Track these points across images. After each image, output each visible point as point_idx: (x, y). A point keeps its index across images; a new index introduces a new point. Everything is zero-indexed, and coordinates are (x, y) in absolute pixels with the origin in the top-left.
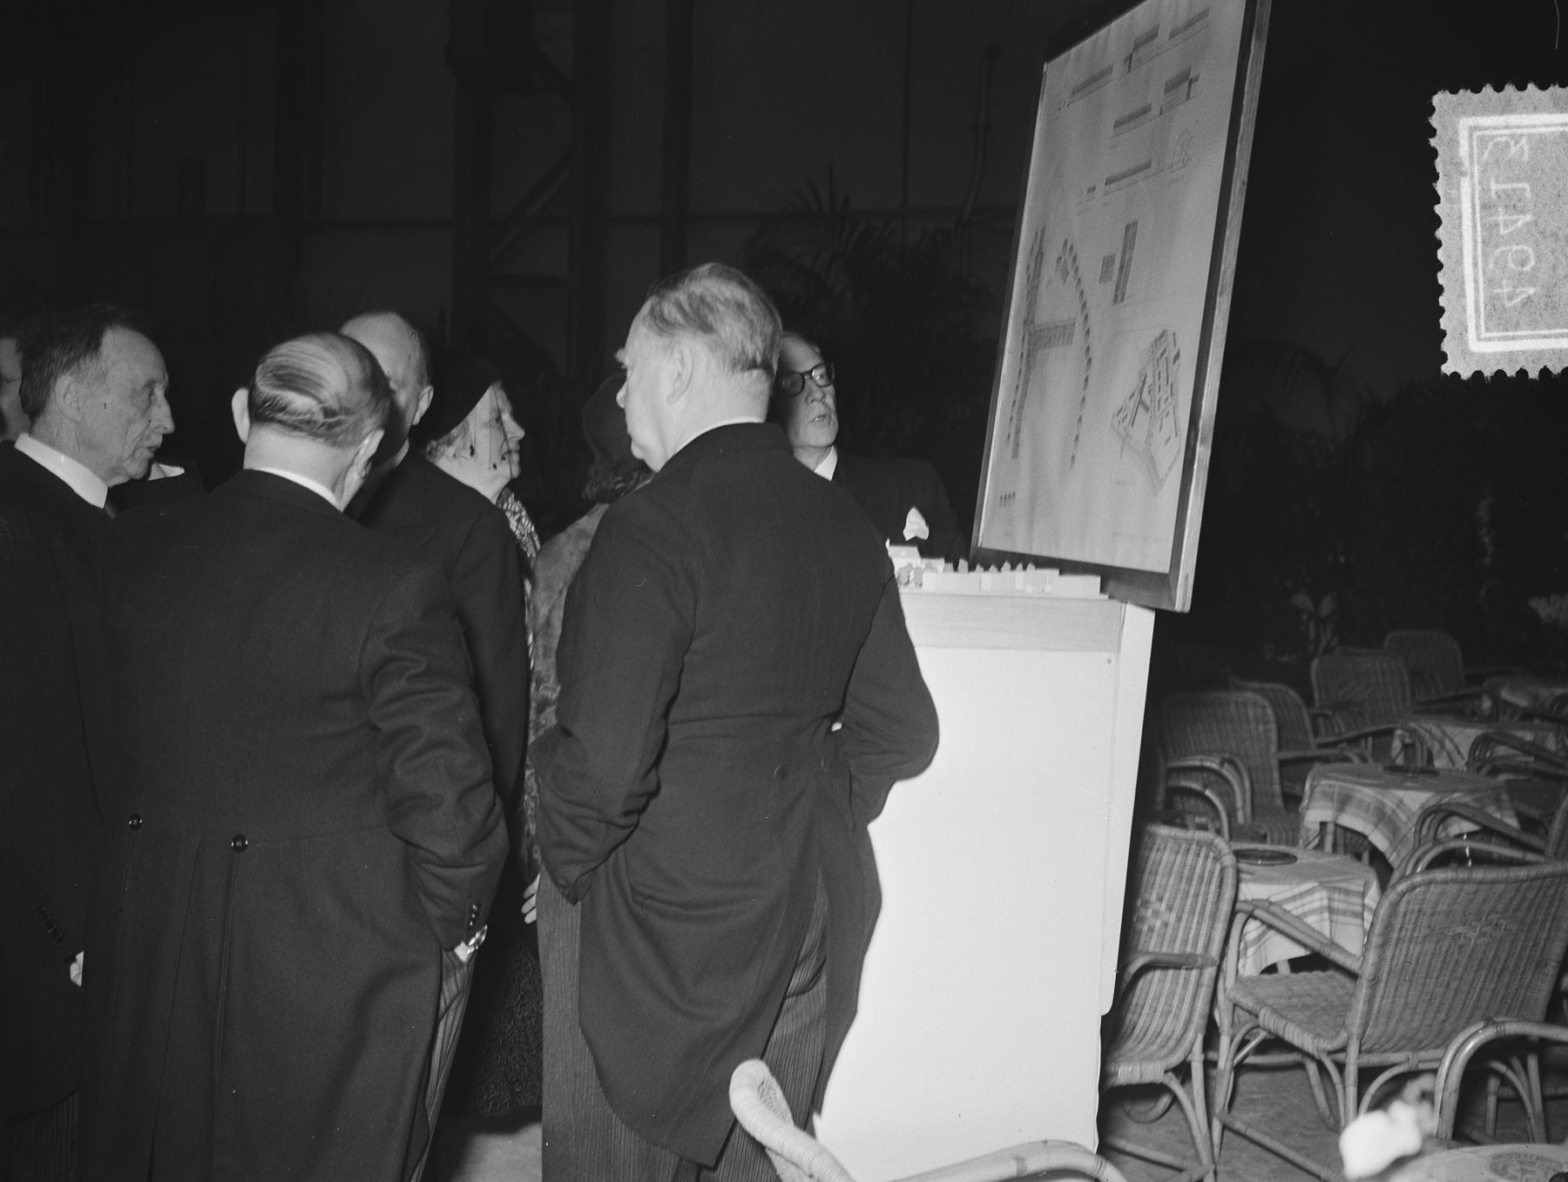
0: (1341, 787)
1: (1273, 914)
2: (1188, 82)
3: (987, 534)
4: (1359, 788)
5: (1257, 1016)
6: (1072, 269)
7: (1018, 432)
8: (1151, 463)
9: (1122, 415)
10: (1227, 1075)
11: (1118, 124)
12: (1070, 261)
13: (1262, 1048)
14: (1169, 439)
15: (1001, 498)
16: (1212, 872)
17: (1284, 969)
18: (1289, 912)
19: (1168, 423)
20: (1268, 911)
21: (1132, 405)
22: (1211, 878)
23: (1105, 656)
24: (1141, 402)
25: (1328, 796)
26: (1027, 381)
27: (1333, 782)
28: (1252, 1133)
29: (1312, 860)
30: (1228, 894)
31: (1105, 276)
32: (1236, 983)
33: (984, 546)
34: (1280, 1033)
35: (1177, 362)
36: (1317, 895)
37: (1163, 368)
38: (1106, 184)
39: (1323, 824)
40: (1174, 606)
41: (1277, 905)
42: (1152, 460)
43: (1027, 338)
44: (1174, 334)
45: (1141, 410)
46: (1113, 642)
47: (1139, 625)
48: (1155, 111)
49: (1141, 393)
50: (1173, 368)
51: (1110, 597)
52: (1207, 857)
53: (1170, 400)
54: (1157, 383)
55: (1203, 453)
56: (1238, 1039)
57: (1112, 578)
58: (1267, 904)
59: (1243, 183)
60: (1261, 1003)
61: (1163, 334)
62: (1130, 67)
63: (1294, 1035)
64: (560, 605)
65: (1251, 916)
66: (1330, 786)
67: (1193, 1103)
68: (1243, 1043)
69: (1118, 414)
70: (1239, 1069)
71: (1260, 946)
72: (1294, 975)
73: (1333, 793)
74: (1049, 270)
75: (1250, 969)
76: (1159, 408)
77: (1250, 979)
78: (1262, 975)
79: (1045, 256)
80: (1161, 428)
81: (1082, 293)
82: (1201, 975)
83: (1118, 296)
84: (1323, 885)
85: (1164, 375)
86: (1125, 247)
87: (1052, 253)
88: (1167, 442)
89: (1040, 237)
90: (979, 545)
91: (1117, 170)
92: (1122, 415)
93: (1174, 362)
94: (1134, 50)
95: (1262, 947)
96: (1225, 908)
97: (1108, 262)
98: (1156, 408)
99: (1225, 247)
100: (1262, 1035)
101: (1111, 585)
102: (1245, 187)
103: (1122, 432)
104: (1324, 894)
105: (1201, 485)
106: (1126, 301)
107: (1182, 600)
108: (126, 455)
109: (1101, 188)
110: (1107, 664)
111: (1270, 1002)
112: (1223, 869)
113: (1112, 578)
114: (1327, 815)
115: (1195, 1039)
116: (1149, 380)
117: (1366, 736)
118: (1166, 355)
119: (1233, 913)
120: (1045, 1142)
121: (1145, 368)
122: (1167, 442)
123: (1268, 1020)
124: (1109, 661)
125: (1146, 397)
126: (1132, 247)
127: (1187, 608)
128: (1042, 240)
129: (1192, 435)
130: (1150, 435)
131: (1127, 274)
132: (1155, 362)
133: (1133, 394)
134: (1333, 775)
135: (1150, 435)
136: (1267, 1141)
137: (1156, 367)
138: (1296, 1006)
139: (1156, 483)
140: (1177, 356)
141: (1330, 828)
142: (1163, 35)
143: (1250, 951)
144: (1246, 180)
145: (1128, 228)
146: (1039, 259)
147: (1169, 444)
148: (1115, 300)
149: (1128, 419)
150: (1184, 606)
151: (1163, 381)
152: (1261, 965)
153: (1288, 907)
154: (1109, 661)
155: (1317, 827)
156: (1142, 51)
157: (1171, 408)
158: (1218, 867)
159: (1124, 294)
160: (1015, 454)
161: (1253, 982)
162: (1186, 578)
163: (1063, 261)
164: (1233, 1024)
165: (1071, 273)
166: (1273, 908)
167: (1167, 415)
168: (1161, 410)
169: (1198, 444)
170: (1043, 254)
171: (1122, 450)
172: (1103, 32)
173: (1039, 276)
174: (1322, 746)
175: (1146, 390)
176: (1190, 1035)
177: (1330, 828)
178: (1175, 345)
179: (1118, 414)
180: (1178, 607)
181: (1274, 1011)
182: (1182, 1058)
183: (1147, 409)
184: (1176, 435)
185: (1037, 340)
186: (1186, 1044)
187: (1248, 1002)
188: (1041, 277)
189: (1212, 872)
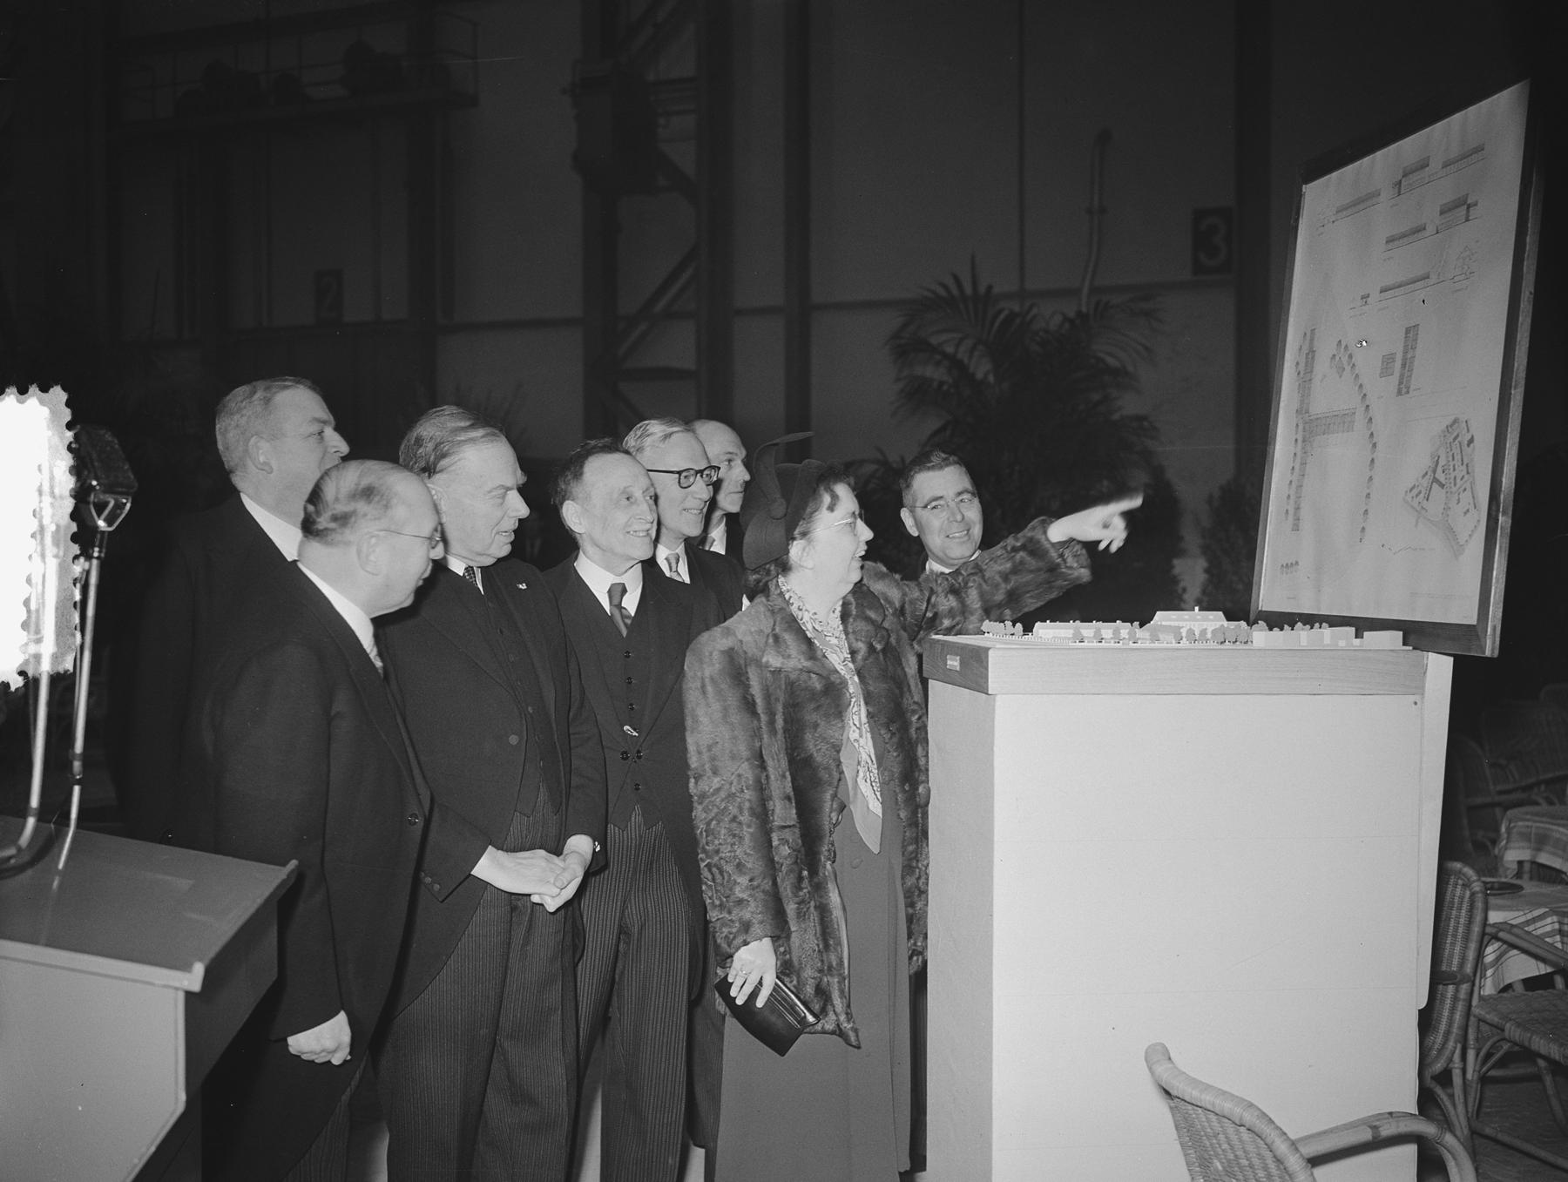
0: (1537, 828)
1: (1517, 936)
2: (1466, 206)
3: (1269, 594)
4: (1555, 827)
5: (1503, 1030)
6: (1349, 364)
7: (1298, 509)
8: (1450, 533)
9: (1415, 491)
10: (1474, 1085)
11: (1390, 240)
12: (1345, 359)
13: (1502, 1063)
14: (1468, 511)
15: (1282, 566)
16: (1462, 898)
17: (1519, 988)
18: (1530, 933)
19: (1466, 497)
20: (1510, 932)
21: (1425, 482)
22: (1461, 903)
23: (1412, 698)
24: (1435, 480)
25: (1526, 837)
26: (1304, 464)
27: (1529, 824)
28: (1500, 1137)
29: (1534, 890)
30: (1478, 918)
31: (1386, 371)
32: (1479, 1001)
33: (1264, 609)
34: (1526, 1044)
35: (1472, 445)
36: (1549, 920)
37: (1456, 451)
38: (1381, 292)
39: (1520, 863)
40: (1484, 653)
41: (1520, 928)
42: (1451, 529)
43: (1301, 427)
44: (1466, 422)
45: (1435, 486)
46: (1415, 685)
47: (1439, 669)
48: (1431, 229)
49: (1434, 472)
50: (1467, 450)
51: (1414, 648)
52: (1456, 885)
53: (1466, 477)
54: (1451, 463)
55: (1504, 521)
56: (1482, 1054)
57: (1418, 635)
58: (1508, 927)
59: (1531, 293)
60: (1507, 1018)
61: (1455, 421)
62: (1399, 192)
63: (1539, 1044)
64: (1469, 650)
65: (1496, 938)
66: (1528, 827)
67: (1454, 1105)
68: (1489, 1055)
69: (1411, 490)
70: (1484, 1080)
71: (1497, 969)
72: (1530, 993)
73: (1530, 833)
74: (1322, 366)
75: (1489, 989)
76: (1455, 485)
77: (1490, 996)
78: (1501, 994)
79: (1317, 354)
80: (1459, 502)
81: (1361, 386)
82: (1457, 991)
83: (1403, 389)
84: (1554, 912)
85: (1458, 457)
86: (1406, 346)
87: (1325, 350)
88: (1465, 513)
89: (1310, 336)
90: (1260, 609)
91: (1390, 281)
92: (1415, 491)
93: (1468, 445)
94: (1403, 177)
95: (1500, 969)
96: (1476, 929)
97: (1388, 360)
98: (1452, 485)
99: (1517, 347)
100: (1506, 1047)
101: (1412, 638)
102: (1532, 296)
103: (1416, 505)
104: (1555, 918)
105: (1503, 550)
106: (1412, 393)
107: (1490, 647)
108: (1042, 572)
109: (1375, 296)
110: (1413, 706)
111: (1514, 1016)
112: (1473, 894)
113: (1418, 635)
114: (1525, 855)
115: (1455, 1048)
116: (1442, 462)
117: (1538, 784)
118: (1459, 439)
119: (1483, 934)
120: (1391, 1114)
121: (1437, 450)
122: (1465, 513)
123: (1512, 1031)
124: (1416, 703)
125: (1441, 476)
126: (1414, 348)
127: (1496, 654)
128: (1312, 340)
129: (1494, 508)
130: (1447, 509)
131: (1411, 370)
132: (1448, 445)
133: (1426, 473)
134: (1528, 817)
135: (1447, 509)
136: (1518, 1143)
137: (1449, 450)
138: (1537, 1020)
139: (1457, 549)
140: (1471, 441)
141: (1527, 867)
142: (1436, 165)
143: (1489, 973)
144: (1533, 291)
145: (1408, 331)
146: (1310, 356)
147: (1467, 515)
148: (1399, 393)
149: (1422, 495)
150: (1493, 652)
151: (1458, 463)
152: (1499, 984)
153: (1530, 928)
154: (1416, 703)
155: (1515, 866)
156: (1414, 177)
157: (1468, 485)
158: (1468, 893)
159: (1409, 388)
160: (1296, 528)
161: (1495, 999)
162: (1494, 628)
163: (1337, 358)
164: (1477, 1040)
165: (1348, 368)
166: (1515, 930)
167: (1465, 490)
168: (1458, 486)
169: (1500, 515)
170: (1314, 352)
171: (1417, 522)
172: (1366, 160)
173: (1312, 372)
174: (1500, 793)
175: (1439, 470)
176: (1451, 1044)
177: (1527, 867)
178: (1468, 430)
179: (1411, 490)
180: (1488, 653)
181: (1519, 1025)
182: (1445, 1065)
183: (1442, 486)
184: (1475, 508)
185: (1311, 429)
186: (1447, 1053)
187: (1493, 1018)
188: (1314, 373)
189: (1462, 898)
